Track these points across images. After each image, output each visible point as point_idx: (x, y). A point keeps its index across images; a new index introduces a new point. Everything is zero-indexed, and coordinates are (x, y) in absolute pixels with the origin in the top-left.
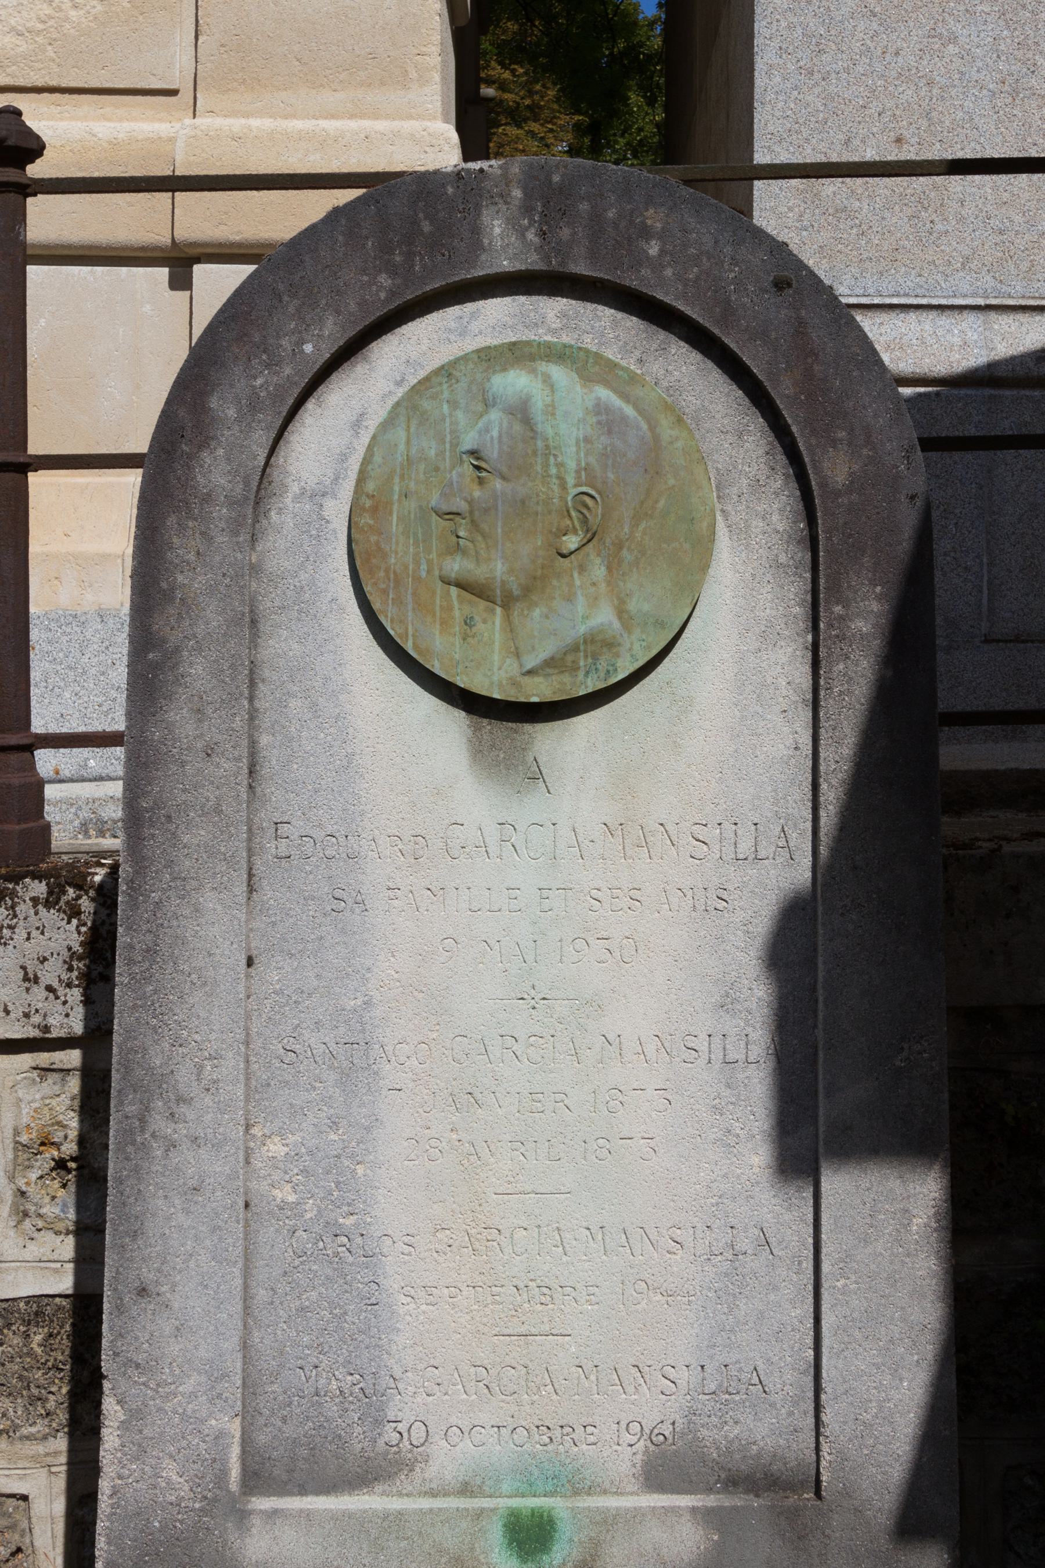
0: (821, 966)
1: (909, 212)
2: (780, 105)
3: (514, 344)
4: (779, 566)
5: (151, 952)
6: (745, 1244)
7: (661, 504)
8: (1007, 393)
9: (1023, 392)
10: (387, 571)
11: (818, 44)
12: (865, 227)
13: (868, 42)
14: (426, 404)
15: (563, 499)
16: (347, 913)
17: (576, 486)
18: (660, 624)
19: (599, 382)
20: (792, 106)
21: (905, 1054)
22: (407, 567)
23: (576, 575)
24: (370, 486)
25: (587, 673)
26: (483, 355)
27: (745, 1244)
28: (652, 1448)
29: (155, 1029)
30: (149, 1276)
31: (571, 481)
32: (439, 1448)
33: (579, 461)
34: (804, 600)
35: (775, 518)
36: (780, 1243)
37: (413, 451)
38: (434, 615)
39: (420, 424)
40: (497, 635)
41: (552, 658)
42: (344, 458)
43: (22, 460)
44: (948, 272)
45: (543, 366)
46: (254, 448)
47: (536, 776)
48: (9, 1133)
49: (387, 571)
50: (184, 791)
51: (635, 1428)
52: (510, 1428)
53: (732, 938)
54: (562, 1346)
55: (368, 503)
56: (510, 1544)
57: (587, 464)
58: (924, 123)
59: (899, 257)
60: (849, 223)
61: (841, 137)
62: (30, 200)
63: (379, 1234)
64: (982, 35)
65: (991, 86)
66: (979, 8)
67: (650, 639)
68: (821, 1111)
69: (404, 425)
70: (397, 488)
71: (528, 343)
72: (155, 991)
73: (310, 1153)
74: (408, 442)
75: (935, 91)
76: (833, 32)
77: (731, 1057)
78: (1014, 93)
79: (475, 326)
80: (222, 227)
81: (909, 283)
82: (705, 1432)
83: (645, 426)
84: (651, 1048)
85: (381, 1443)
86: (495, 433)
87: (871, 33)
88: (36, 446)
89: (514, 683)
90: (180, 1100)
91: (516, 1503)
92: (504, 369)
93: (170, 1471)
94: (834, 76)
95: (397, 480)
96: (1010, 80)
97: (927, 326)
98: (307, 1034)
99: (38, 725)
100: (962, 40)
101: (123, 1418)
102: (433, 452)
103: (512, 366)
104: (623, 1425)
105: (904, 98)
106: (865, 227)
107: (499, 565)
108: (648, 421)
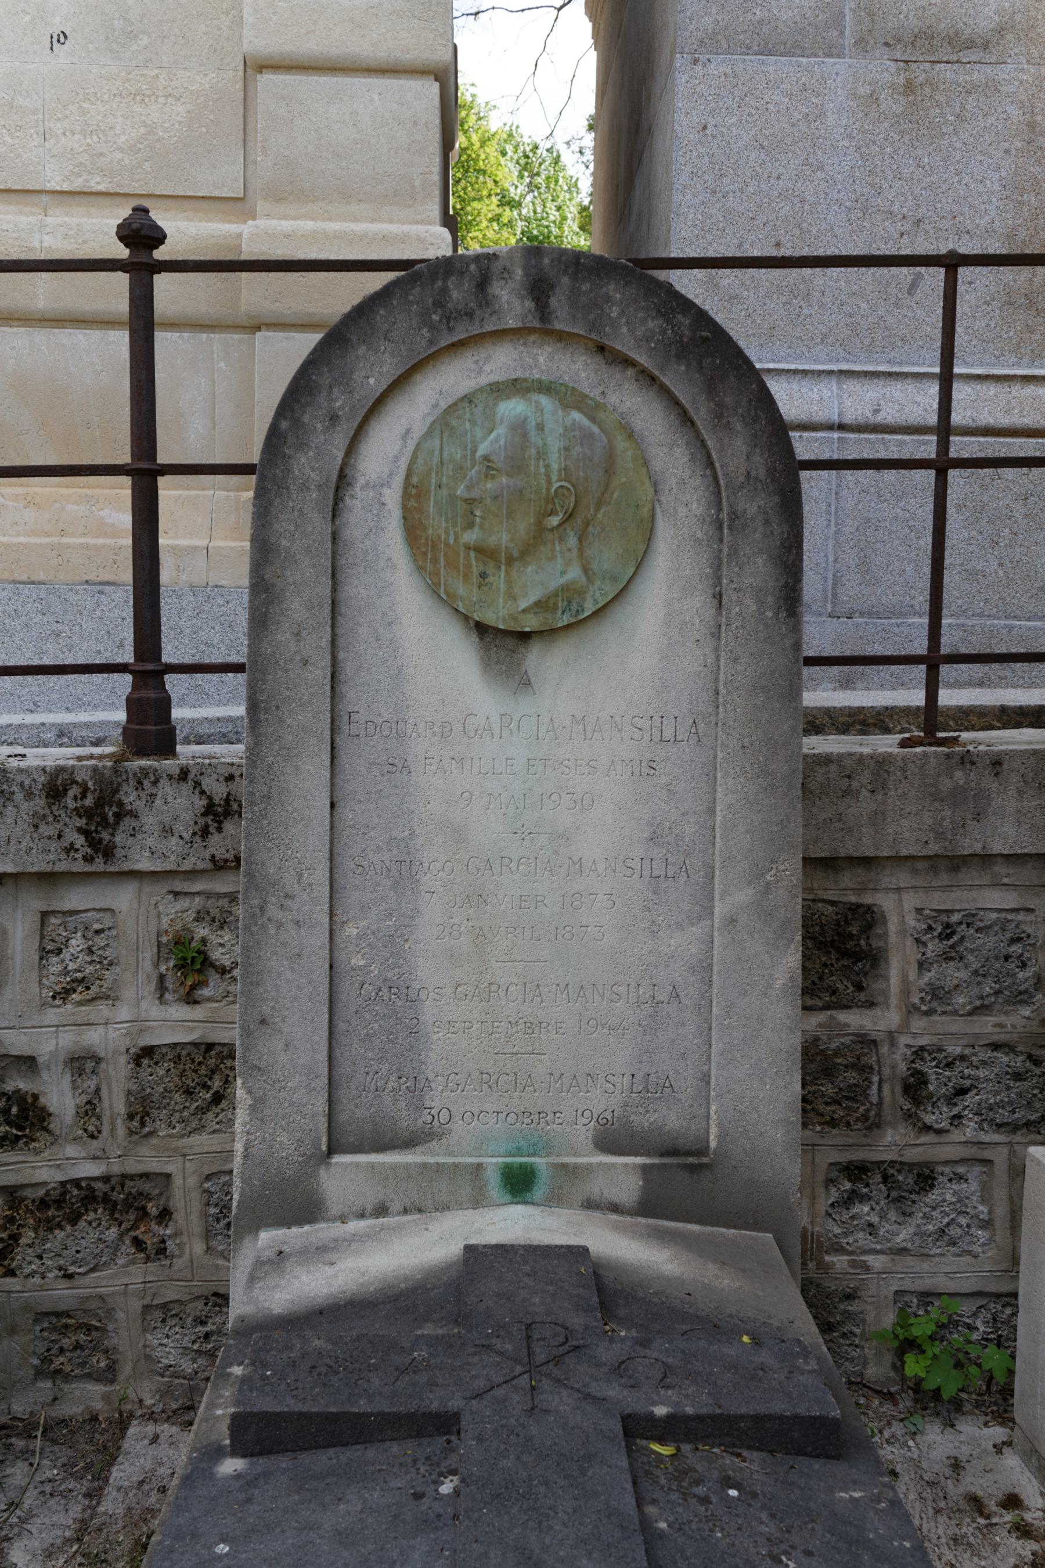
0: (719, 813)
1: (784, 299)
2: (691, 216)
3: (516, 380)
4: (697, 540)
5: (267, 797)
6: (663, 996)
7: (615, 496)
8: (852, 436)
9: (862, 436)
10: (427, 539)
11: (720, 170)
12: (750, 311)
13: (758, 169)
14: (454, 422)
15: (548, 489)
16: (398, 774)
17: (559, 480)
18: (614, 579)
19: (574, 408)
20: (700, 217)
21: (773, 872)
22: (440, 537)
23: (557, 542)
24: (415, 480)
25: (563, 612)
26: (493, 387)
27: (663, 996)
28: (599, 1127)
29: (269, 850)
30: (266, 1010)
31: (554, 478)
32: (458, 1126)
33: (560, 463)
34: (712, 563)
35: (695, 506)
36: (686, 995)
37: (445, 455)
38: (459, 571)
39: (450, 436)
40: (502, 586)
41: (540, 601)
42: (396, 459)
43: (153, 467)
44: (811, 345)
45: (535, 397)
46: (335, 451)
47: (527, 683)
48: (154, 935)
49: (427, 539)
50: (287, 689)
51: (587, 1114)
52: (504, 1114)
53: (658, 794)
54: (541, 1061)
55: (414, 491)
56: (505, 1185)
57: (566, 466)
58: (797, 232)
59: (775, 334)
60: (740, 307)
61: (735, 241)
62: (156, 277)
63: (418, 987)
64: (842, 164)
65: (848, 204)
66: (841, 143)
67: (607, 589)
68: (717, 910)
69: (438, 437)
70: (433, 481)
71: (525, 380)
72: (269, 824)
73: (373, 933)
74: (441, 449)
75: (806, 207)
76: (732, 161)
77: (656, 873)
78: (865, 210)
79: (487, 368)
80: (277, 304)
81: (782, 353)
82: (633, 1117)
83: (605, 440)
84: (601, 868)
85: (420, 1122)
86: (502, 443)
87: (760, 161)
88: (162, 458)
89: (514, 618)
90: (287, 896)
91: (509, 1160)
92: (508, 398)
93: (283, 1138)
94: (731, 194)
95: (433, 475)
96: (862, 199)
97: (795, 386)
98: (371, 855)
99: (166, 659)
100: (828, 168)
101: (251, 1102)
102: (458, 456)
103: (514, 395)
104: (579, 1113)
105: (783, 212)
106: (750, 311)
107: (504, 536)
108: (608, 437)
